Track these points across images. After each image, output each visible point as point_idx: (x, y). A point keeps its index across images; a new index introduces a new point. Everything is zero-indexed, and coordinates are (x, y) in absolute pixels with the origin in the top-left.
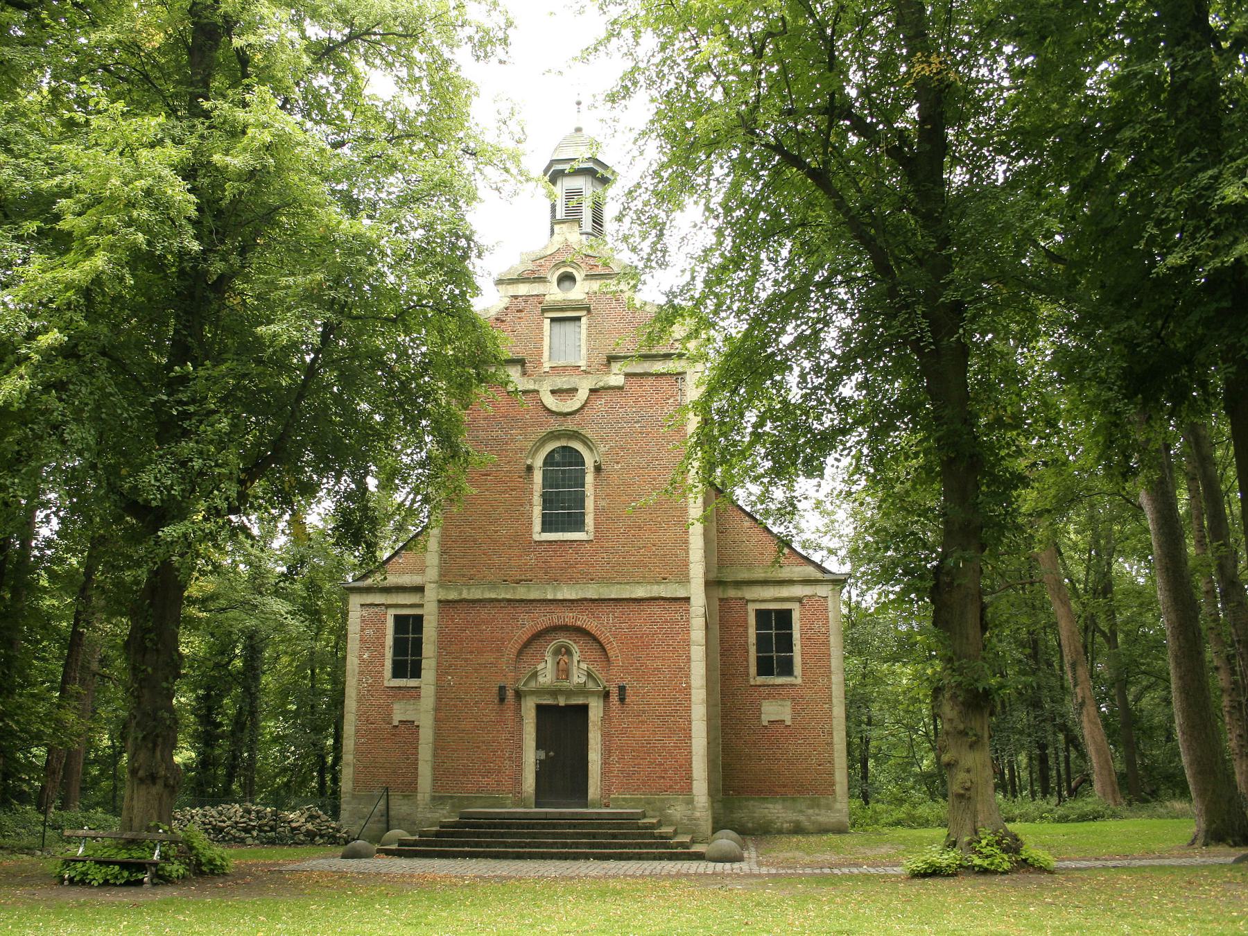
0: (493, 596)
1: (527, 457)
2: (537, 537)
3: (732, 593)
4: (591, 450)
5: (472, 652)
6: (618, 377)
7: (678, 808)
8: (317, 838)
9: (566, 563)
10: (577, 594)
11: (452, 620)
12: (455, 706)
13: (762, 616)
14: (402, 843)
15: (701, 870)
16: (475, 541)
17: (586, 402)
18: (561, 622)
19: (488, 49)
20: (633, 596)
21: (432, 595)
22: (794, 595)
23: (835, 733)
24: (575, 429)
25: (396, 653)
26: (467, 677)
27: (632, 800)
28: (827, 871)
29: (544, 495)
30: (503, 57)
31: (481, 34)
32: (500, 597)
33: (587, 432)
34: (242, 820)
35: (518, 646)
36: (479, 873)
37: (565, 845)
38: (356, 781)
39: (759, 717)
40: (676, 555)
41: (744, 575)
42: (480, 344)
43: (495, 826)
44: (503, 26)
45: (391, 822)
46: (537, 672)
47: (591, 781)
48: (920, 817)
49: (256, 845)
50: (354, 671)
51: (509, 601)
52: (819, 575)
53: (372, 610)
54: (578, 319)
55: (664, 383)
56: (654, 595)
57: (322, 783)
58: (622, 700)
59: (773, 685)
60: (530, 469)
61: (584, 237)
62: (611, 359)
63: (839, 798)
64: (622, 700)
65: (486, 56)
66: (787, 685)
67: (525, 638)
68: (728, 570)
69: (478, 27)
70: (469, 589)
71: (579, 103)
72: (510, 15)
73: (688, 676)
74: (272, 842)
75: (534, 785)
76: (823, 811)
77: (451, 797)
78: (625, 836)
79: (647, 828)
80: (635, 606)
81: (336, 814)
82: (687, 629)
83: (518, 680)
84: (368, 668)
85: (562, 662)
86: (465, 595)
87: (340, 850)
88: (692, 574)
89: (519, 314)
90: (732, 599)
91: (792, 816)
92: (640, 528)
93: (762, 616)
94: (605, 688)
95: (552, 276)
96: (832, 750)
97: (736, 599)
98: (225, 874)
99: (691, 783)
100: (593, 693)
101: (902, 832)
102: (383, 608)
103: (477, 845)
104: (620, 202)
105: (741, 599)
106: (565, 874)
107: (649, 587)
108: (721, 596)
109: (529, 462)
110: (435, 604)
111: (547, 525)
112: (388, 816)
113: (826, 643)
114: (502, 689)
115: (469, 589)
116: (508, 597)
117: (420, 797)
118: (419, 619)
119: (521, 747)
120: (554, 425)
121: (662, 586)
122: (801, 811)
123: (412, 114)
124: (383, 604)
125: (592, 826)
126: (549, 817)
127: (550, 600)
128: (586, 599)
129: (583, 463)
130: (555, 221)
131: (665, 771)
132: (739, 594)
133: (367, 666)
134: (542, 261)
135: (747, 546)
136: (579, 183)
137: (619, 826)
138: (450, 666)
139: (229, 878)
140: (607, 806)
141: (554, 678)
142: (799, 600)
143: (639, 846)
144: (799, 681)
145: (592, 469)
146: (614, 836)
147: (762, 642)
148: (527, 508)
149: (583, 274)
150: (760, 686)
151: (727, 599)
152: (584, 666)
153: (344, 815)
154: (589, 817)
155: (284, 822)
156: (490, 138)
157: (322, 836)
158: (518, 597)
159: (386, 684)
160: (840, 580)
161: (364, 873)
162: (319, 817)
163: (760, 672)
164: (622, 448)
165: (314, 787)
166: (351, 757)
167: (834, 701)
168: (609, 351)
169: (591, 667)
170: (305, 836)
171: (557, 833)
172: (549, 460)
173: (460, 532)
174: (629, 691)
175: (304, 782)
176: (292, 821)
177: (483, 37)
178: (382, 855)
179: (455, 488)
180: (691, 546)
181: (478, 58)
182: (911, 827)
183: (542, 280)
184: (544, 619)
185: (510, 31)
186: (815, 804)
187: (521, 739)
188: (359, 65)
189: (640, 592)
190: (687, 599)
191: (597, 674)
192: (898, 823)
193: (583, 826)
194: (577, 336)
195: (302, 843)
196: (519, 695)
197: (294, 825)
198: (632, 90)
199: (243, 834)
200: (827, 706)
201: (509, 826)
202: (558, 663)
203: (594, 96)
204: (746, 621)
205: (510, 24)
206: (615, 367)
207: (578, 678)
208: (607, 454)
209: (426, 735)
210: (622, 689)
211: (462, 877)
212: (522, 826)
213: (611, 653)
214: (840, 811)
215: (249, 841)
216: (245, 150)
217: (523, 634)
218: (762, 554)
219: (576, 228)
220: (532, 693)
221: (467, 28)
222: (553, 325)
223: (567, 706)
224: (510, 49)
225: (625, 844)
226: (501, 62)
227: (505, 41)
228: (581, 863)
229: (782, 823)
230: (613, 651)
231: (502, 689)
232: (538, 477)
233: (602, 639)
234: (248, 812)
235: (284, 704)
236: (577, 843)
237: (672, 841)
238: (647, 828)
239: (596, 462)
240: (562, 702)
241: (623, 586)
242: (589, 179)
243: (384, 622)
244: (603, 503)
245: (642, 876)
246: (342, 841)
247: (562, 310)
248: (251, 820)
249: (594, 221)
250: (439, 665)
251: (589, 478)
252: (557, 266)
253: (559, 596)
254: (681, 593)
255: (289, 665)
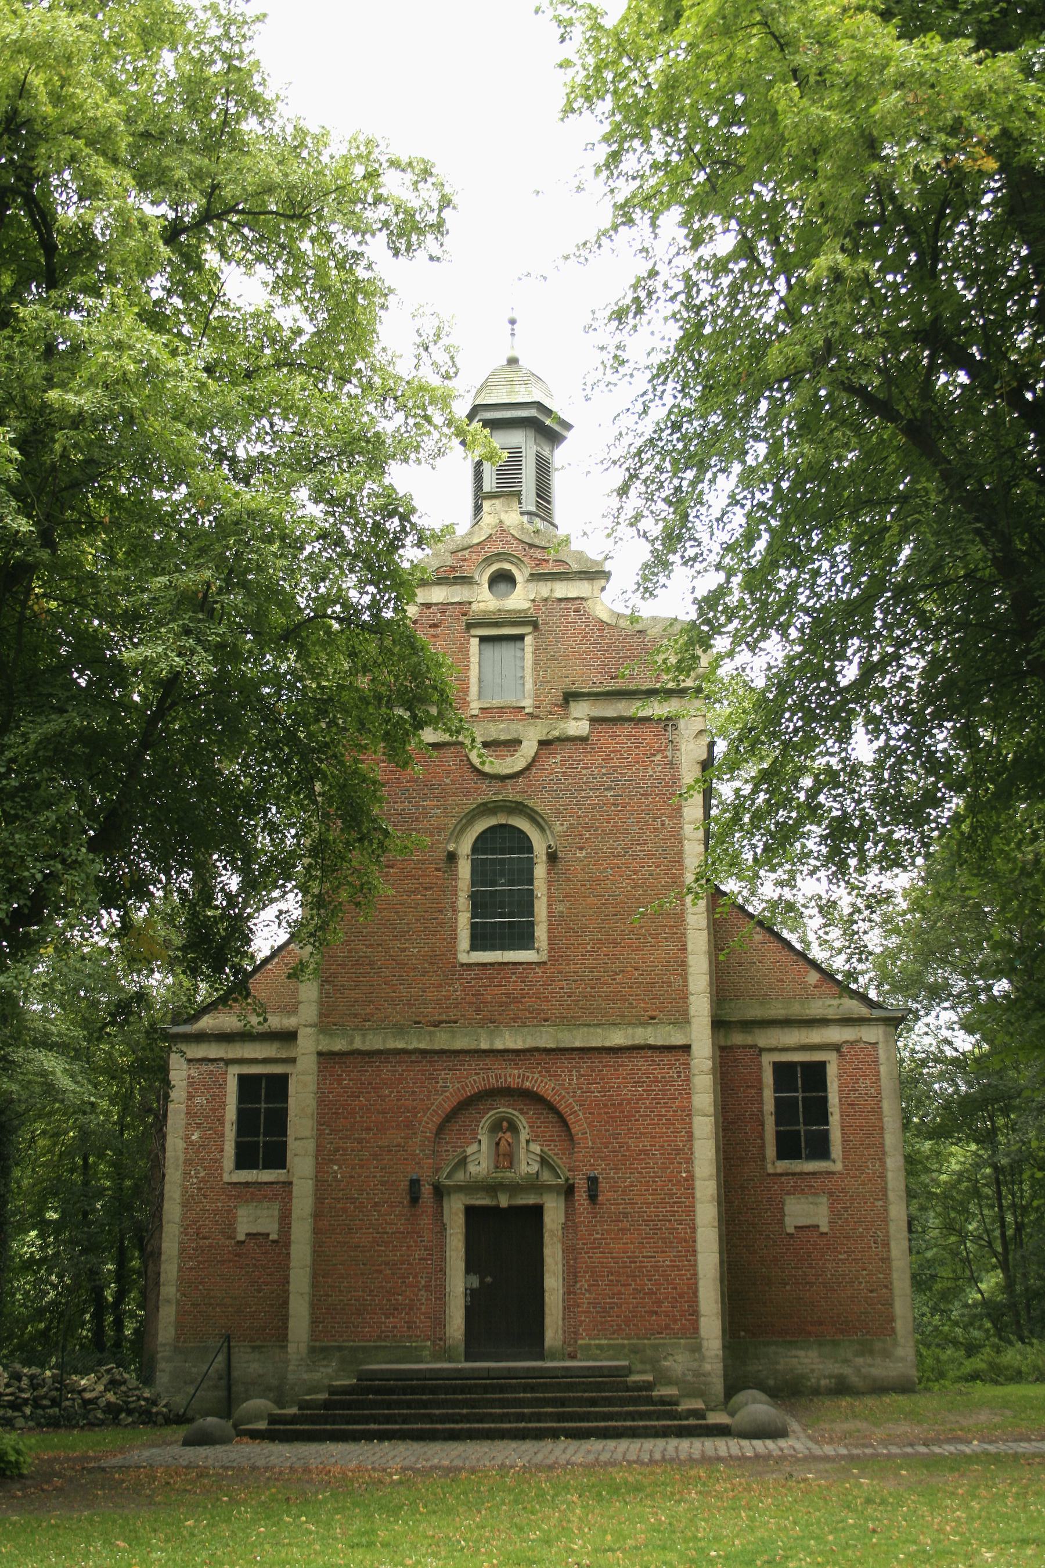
0: (400, 1045)
1: (448, 841)
2: (463, 958)
3: (738, 1039)
4: (542, 829)
5: (368, 1129)
6: (580, 723)
7: (679, 1358)
8: (123, 1415)
9: (508, 995)
10: (524, 1041)
11: (339, 1081)
12: (344, 1210)
13: (783, 1071)
14: (273, 1420)
15: (735, 1451)
16: (371, 964)
17: (534, 760)
18: (501, 1083)
19: (414, 238)
20: (607, 1044)
21: (307, 1045)
22: (829, 1041)
23: (893, 1244)
24: (518, 799)
25: (240, 1133)
26: (361, 1167)
27: (610, 1347)
28: (923, 1449)
29: (473, 896)
30: (436, 251)
31: (401, 216)
32: (410, 1047)
33: (537, 804)
34: (8, 1391)
35: (437, 1120)
36: (407, 1463)
37: (521, 1418)
38: (180, 1326)
39: (781, 1222)
40: (669, 984)
41: (755, 1012)
42: (416, 674)
43: (413, 1390)
44: (436, 206)
45: (234, 1389)
46: (466, 1157)
47: (548, 1321)
48: (1007, 1368)
49: (30, 1429)
50: (177, 1159)
51: (424, 1052)
52: (864, 1011)
53: (204, 1067)
54: (521, 638)
55: (647, 733)
56: (638, 1041)
57: (98, 1331)
58: (593, 1197)
59: (801, 1174)
60: (452, 857)
61: (525, 518)
62: (570, 697)
63: (901, 1340)
64: (593, 1197)
65: (408, 250)
66: (821, 1173)
67: (448, 1107)
68: (733, 1005)
69: (398, 207)
70: (364, 1036)
71: (513, 322)
72: (447, 190)
73: (690, 1161)
74: (54, 1424)
75: (463, 1327)
76: (878, 1361)
77: (340, 1348)
78: (609, 1402)
79: (640, 1389)
80: (607, 1058)
81: (147, 1378)
82: (687, 1092)
83: (438, 1170)
84: (196, 1154)
85: (503, 1143)
86: (358, 1044)
87: (181, 1432)
88: (693, 1010)
89: (432, 631)
90: (738, 1047)
91: (835, 1368)
92: (616, 944)
93: (783, 1071)
94: (567, 1179)
95: (481, 575)
96: (890, 1268)
97: (744, 1047)
98: (21, 1476)
99: (697, 1321)
100: (549, 1188)
101: (981, 1390)
102: (222, 1064)
103: (388, 1419)
104: (625, 466)
105: (751, 1047)
106: (536, 1460)
107: (630, 1031)
108: (723, 1044)
109: (451, 847)
110: (314, 1058)
111: (480, 939)
112: (229, 1379)
113: (878, 1111)
114: (415, 1185)
115: (364, 1036)
116: (422, 1046)
117: (292, 1348)
118: (278, 1085)
119: (443, 1271)
120: (488, 793)
121: (650, 1029)
122: (846, 1361)
123: (287, 334)
124: (221, 1059)
125: (559, 1388)
126: (492, 1375)
127: (484, 1051)
128: (537, 1049)
129: (530, 849)
130: (480, 497)
131: (659, 1303)
132: (749, 1040)
133: (197, 1152)
134: (466, 553)
135: (758, 970)
136: (517, 438)
137: (599, 1387)
138: (337, 1150)
139: (29, 1482)
140: (572, 1357)
141: (492, 1166)
142: (837, 1048)
143: (632, 1416)
144: (838, 1167)
145: (544, 858)
146: (593, 1402)
147: (784, 1110)
148: (450, 914)
149: (527, 572)
150: (781, 1175)
151: (731, 1047)
152: (536, 1148)
153: (163, 1377)
154: (542, 1373)
155: (72, 1392)
156: (404, 369)
157: (130, 1412)
158: (437, 1047)
159: (226, 1178)
160: (895, 1019)
161: (233, 1468)
162: (124, 1382)
163: (781, 1155)
164: (587, 827)
165: (86, 1337)
166: (173, 1289)
167: (891, 1195)
168: (565, 685)
169: (546, 1149)
170: (104, 1412)
171: (508, 1399)
172: (481, 844)
173: (350, 951)
174: (603, 1185)
175: (70, 1329)
176: (84, 1390)
177: (404, 221)
178: (245, 1439)
179: (362, 885)
180: (691, 970)
181: (396, 253)
182: (996, 1382)
183: (466, 581)
184: (475, 1079)
185: (446, 213)
186: (866, 1349)
187: (443, 1259)
188: (211, 257)
189: (617, 1038)
190: (686, 1048)
191: (560, 1162)
192: (974, 1377)
193: (545, 1388)
194: (519, 663)
195: (101, 1423)
196: (440, 1192)
197: (88, 1395)
198: (645, 303)
199: (10, 1413)
200: (880, 1203)
201: (434, 1390)
202: (498, 1144)
203: (593, 312)
204: (760, 1080)
205: (445, 202)
206: (581, 709)
207: (527, 1166)
208: (565, 835)
209: (301, 1252)
210: (593, 1181)
211: (384, 1470)
212: (455, 1390)
213: (575, 1129)
214: (903, 1359)
215: (20, 1422)
216: (91, 381)
217: (445, 1101)
218: (782, 981)
219: (515, 505)
220: (459, 1189)
221: (381, 207)
222: (483, 646)
223: (511, 1208)
224: (446, 240)
225: (611, 1413)
226: (431, 258)
227: (438, 227)
228: (548, 1445)
229: (819, 1379)
230: (579, 1125)
231: (415, 1185)
232: (464, 869)
233: (562, 1107)
234: (17, 1377)
235: (41, 1210)
236: (539, 1414)
237: (680, 1408)
238: (640, 1389)
239: (549, 847)
240: (504, 1201)
241: (592, 1030)
242: (531, 434)
243: (223, 1086)
244: (561, 908)
245: (652, 1461)
246: (160, 1419)
247: (496, 624)
248: (22, 1390)
249: (538, 496)
250: (319, 1149)
251: (540, 871)
252: (488, 561)
253: (499, 1045)
254: (678, 1039)
255: (49, 1151)
